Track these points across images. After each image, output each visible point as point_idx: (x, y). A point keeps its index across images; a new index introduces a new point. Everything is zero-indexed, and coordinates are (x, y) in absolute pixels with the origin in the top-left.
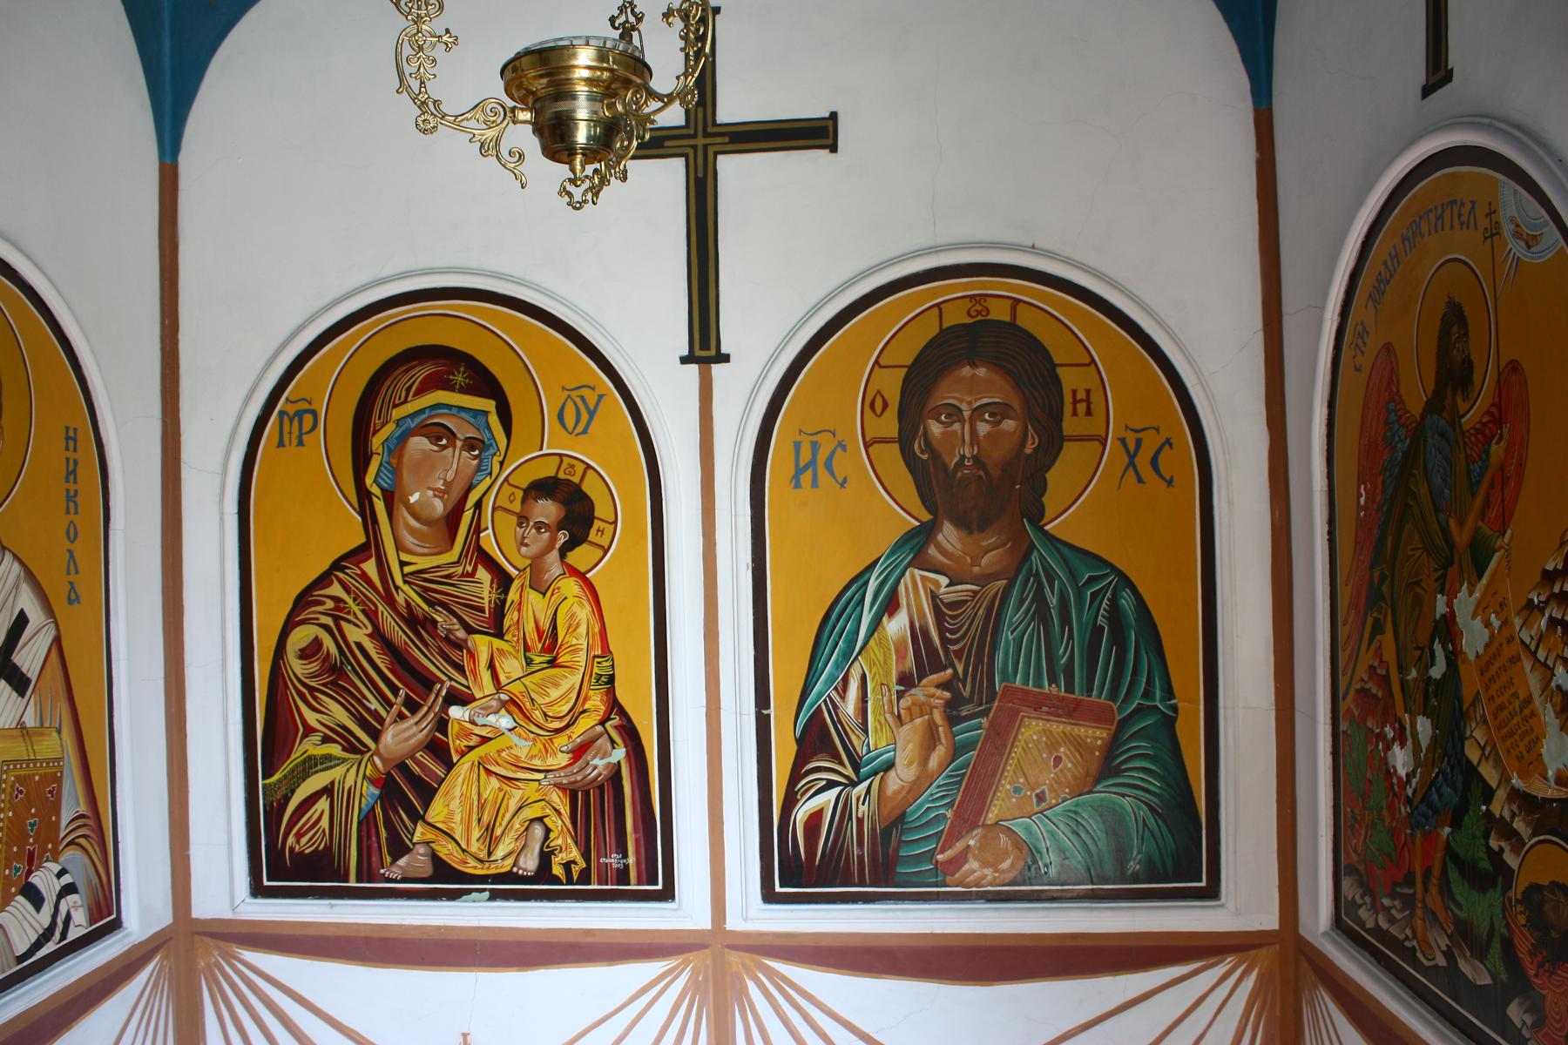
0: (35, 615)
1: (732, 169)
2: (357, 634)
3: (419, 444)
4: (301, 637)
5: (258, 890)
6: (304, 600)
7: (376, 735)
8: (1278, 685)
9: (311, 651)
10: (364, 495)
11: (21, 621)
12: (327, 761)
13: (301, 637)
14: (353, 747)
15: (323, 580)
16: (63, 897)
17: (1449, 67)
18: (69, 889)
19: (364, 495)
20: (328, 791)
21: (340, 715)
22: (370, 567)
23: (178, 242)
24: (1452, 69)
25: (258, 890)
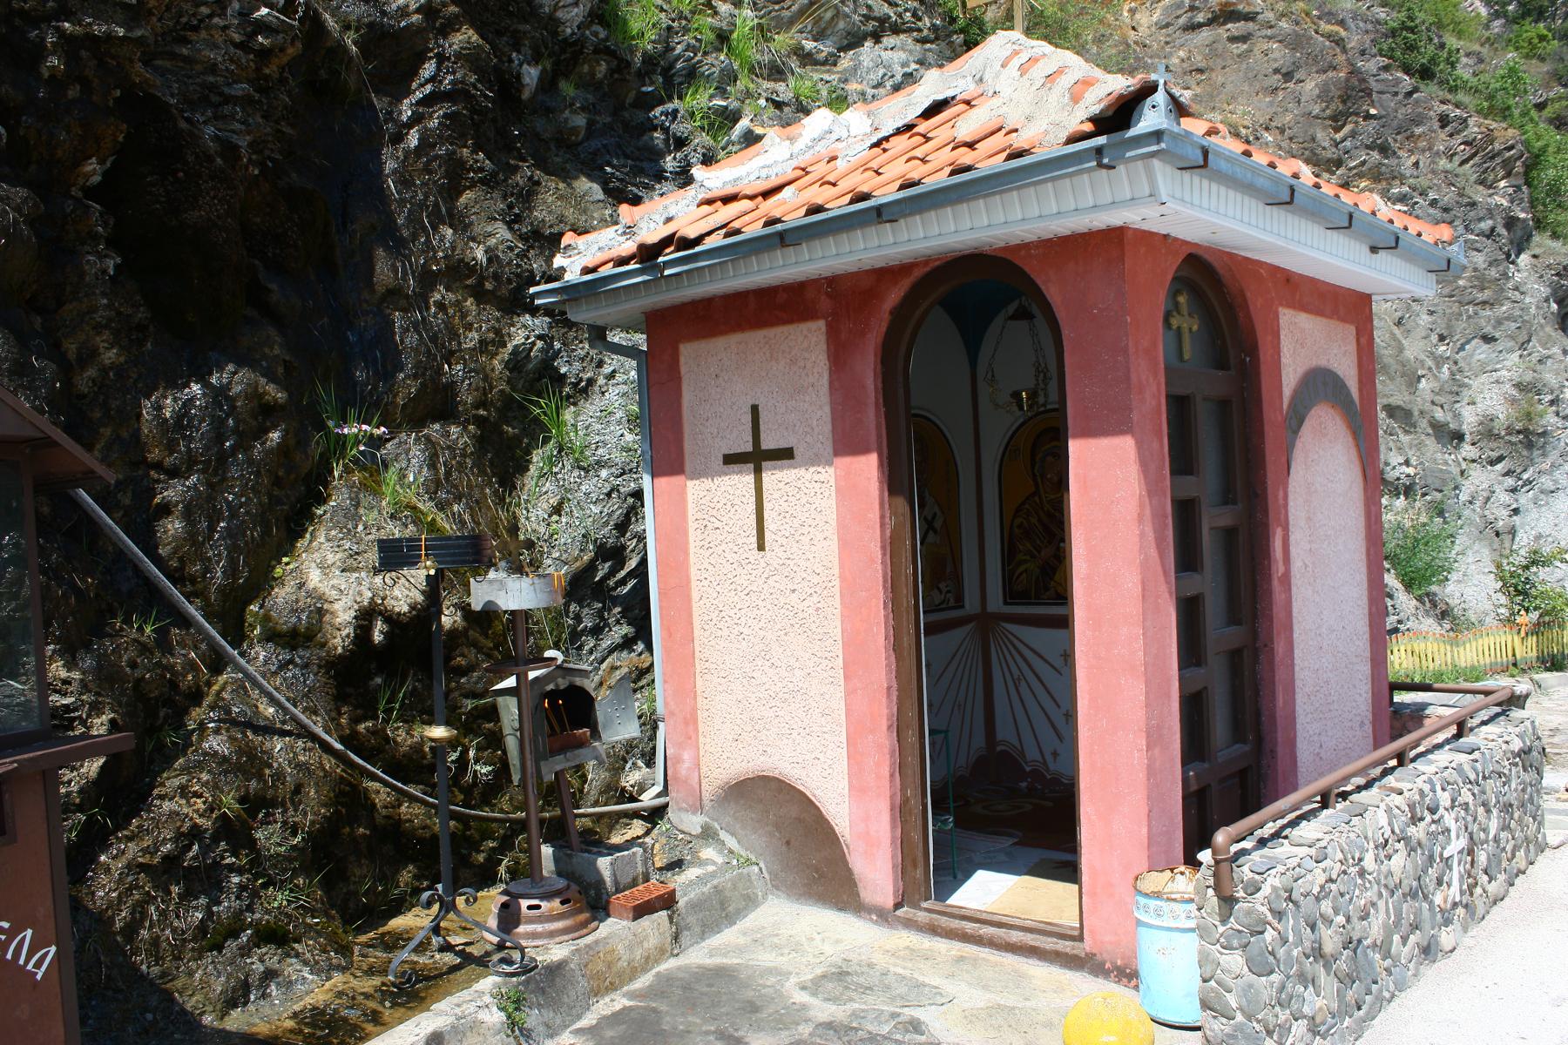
0: (939, 513)
1: (749, 448)
2: (1034, 520)
3: (1050, 459)
4: (1018, 521)
5: (1006, 603)
6: (1018, 510)
7: (1039, 552)
8: (1374, 609)
9: (1020, 526)
10: (1034, 475)
11: (935, 514)
12: (1025, 561)
13: (1018, 521)
14: (1033, 556)
15: (1023, 503)
16: (235, 1006)
17: (1088, 127)
18: (949, 592)
19: (1034, 475)
20: (1026, 571)
21: (1028, 545)
22: (1037, 499)
23: (1252, 331)
24: (1091, 120)
25: (1006, 603)
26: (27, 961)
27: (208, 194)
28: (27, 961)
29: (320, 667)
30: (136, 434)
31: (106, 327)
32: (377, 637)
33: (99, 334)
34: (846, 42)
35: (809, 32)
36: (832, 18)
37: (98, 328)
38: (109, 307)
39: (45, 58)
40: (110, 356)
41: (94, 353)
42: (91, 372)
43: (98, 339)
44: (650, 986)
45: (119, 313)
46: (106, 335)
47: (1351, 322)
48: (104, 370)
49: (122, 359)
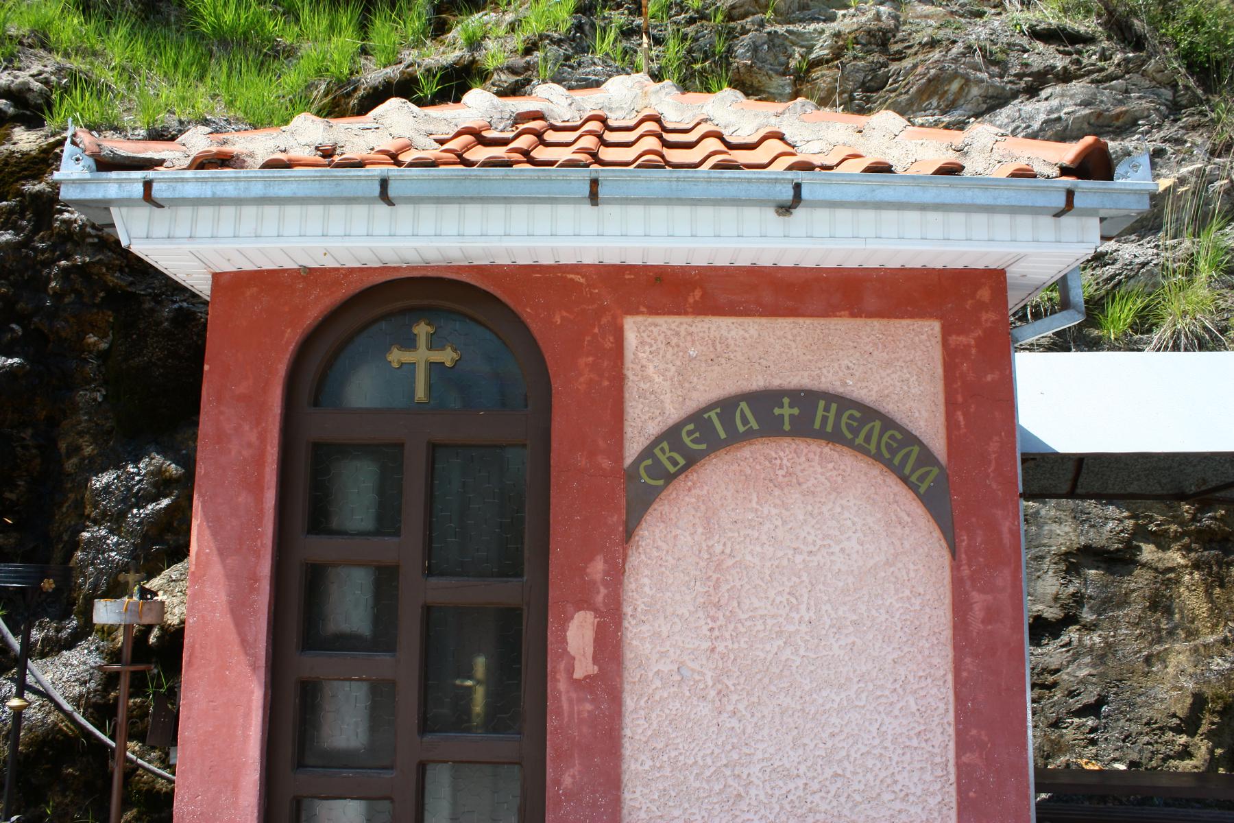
26: (913, 471)
27: (152, 346)
28: (913, 471)
29: (107, 654)
30: (83, 498)
31: (88, 432)
32: (152, 639)
33: (82, 437)
34: (985, 106)
35: (937, 107)
36: (961, 88)
37: (81, 434)
38: (90, 420)
39: (49, 283)
40: (88, 450)
41: (78, 449)
42: (75, 460)
43: (81, 440)
44: (620, 767)
45: (97, 425)
46: (87, 437)
47: (931, 316)
48: (84, 459)
49: (95, 452)
